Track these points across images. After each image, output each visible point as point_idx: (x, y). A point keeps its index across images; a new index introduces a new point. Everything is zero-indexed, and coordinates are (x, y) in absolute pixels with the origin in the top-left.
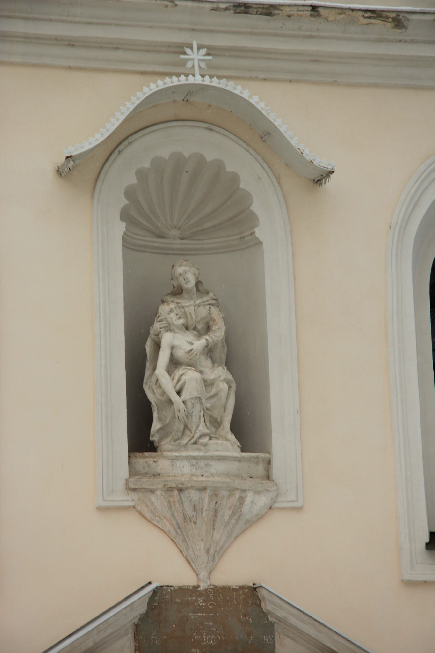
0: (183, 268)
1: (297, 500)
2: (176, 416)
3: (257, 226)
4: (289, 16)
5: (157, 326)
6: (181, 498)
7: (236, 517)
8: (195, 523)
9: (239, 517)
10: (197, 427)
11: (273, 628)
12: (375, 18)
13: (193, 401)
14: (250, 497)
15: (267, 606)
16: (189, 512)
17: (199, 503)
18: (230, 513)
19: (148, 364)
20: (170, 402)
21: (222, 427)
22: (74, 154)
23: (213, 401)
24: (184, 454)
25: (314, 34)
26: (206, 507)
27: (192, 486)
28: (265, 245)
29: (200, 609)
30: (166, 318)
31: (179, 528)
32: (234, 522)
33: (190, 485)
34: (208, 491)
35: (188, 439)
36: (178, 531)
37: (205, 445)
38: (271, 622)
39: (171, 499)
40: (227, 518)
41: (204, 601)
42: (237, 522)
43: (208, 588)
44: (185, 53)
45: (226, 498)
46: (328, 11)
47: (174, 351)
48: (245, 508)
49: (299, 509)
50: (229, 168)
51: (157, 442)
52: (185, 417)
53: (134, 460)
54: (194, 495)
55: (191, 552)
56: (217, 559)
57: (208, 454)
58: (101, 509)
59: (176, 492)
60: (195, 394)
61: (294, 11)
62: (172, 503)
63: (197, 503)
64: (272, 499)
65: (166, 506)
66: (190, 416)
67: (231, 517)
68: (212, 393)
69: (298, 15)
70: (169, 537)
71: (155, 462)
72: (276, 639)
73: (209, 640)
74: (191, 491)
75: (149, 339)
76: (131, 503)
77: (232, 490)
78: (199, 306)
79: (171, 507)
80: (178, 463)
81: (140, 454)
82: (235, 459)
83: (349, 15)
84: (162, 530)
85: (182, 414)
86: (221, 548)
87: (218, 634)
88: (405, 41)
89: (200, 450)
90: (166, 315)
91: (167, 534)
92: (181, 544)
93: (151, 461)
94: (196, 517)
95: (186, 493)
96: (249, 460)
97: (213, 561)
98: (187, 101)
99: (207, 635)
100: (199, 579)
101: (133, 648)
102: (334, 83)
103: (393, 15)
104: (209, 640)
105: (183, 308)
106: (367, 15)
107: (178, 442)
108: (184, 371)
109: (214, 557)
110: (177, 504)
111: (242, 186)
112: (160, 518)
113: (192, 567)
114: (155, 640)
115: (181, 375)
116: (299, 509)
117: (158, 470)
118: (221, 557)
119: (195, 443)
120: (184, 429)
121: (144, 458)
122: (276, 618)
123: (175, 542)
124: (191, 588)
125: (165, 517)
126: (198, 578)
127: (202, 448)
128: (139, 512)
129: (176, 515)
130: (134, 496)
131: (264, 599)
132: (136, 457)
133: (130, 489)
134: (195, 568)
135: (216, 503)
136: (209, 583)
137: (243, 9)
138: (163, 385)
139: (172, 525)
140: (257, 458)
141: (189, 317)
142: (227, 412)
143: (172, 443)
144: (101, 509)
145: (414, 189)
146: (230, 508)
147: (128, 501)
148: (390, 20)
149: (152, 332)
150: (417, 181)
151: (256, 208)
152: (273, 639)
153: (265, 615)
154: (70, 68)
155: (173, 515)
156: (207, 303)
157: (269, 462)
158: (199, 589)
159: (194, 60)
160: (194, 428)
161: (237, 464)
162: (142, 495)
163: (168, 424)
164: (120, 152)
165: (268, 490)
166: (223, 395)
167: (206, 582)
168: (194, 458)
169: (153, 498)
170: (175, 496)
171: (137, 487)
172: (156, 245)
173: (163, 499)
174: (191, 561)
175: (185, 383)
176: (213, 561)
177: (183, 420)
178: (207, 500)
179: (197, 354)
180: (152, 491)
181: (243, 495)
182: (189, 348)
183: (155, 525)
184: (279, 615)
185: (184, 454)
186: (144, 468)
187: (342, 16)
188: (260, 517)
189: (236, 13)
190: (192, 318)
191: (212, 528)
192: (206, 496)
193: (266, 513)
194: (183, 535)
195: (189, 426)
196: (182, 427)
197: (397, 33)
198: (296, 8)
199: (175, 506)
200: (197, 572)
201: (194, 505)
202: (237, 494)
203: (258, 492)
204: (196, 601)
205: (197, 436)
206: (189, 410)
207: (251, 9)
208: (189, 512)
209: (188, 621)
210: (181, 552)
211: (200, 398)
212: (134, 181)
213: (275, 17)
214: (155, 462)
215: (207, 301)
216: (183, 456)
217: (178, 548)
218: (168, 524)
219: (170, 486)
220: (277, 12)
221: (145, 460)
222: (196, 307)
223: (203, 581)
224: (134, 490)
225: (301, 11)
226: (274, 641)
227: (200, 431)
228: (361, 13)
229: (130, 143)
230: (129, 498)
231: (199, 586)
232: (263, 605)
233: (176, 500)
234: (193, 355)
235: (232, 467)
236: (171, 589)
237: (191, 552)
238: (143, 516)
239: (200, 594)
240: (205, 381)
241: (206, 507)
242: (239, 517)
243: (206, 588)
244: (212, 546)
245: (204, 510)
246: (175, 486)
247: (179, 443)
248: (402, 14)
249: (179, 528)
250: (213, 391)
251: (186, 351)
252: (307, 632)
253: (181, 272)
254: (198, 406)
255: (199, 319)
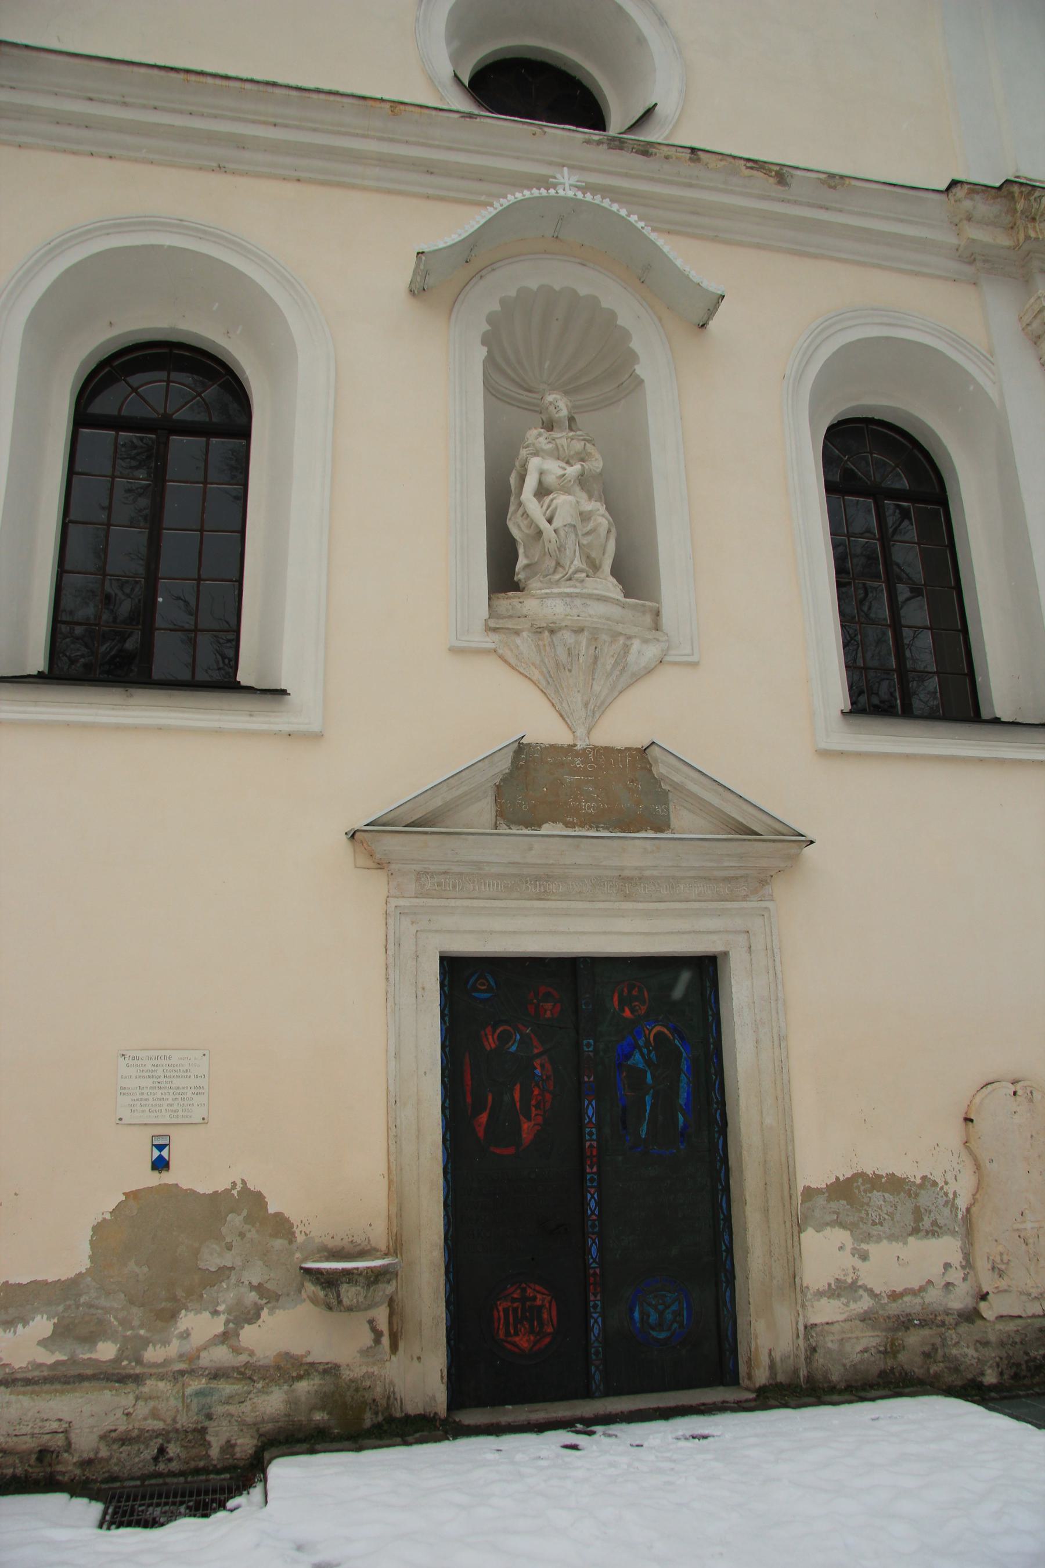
0: (554, 396)
1: (693, 655)
2: (546, 550)
3: (638, 363)
4: (667, 158)
5: (523, 452)
6: (552, 641)
7: (620, 668)
8: (570, 671)
9: (624, 668)
10: (572, 563)
11: (668, 798)
12: (757, 169)
13: (566, 529)
14: (636, 645)
15: (660, 770)
16: (563, 657)
17: (575, 648)
18: (613, 662)
19: (512, 499)
20: (540, 533)
21: (601, 570)
22: (426, 250)
23: (590, 538)
24: (556, 590)
25: (694, 182)
26: (583, 652)
27: (566, 626)
28: (647, 384)
29: (577, 772)
30: (534, 444)
31: (551, 677)
32: (618, 673)
33: (564, 624)
34: (586, 633)
35: (561, 575)
36: (549, 680)
37: (582, 581)
38: (665, 790)
39: (540, 643)
40: (609, 667)
41: (582, 762)
42: (621, 674)
43: (587, 748)
44: (555, 178)
45: (607, 644)
46: (708, 155)
47: (543, 478)
48: (631, 658)
49: (695, 665)
50: (604, 305)
51: (523, 581)
52: (556, 549)
53: (495, 602)
54: (568, 637)
55: (565, 705)
56: (597, 716)
57: (585, 591)
58: (454, 650)
59: (547, 633)
60: (569, 520)
61: (671, 152)
62: (542, 647)
63: (573, 646)
64: (663, 650)
65: (534, 650)
66: (563, 549)
67: (614, 667)
68: (588, 528)
69: (677, 158)
70: (538, 687)
71: (520, 602)
72: (671, 810)
73: (589, 808)
74: (565, 632)
75: (514, 471)
76: (493, 646)
77: (615, 635)
78: (572, 439)
79: (540, 651)
80: (549, 602)
81: (503, 594)
82: (617, 602)
83: (731, 163)
84: (529, 678)
85: (552, 547)
86: (602, 703)
87: (600, 801)
88: (789, 201)
89: (576, 587)
90: (534, 441)
91: (535, 684)
92: (553, 695)
93: (515, 602)
94: (572, 664)
95: (559, 635)
96: (634, 607)
97: (593, 718)
98: (557, 237)
99: (586, 802)
100: (575, 737)
101: (494, 814)
102: (715, 239)
103: (777, 168)
104: (589, 808)
105: (554, 440)
106: (749, 164)
107: (548, 577)
108: (555, 495)
109: (594, 712)
110: (548, 648)
111: (619, 322)
112: (527, 664)
113: (567, 723)
114: (521, 805)
115: (552, 500)
116: (695, 665)
117: (525, 612)
118: (603, 713)
119: (570, 579)
120: (556, 568)
121: (507, 599)
122: (671, 785)
123: (545, 694)
124: (565, 746)
125: (533, 664)
126: (574, 736)
127: (578, 584)
128: (501, 657)
129: (546, 661)
130: (495, 637)
131: (656, 761)
132: (498, 598)
133: (489, 629)
134: (570, 724)
135: (596, 648)
136: (587, 742)
137: (617, 143)
138: (530, 512)
139: (542, 673)
140: (643, 605)
141: (561, 449)
142: (606, 555)
143: (541, 579)
144: (454, 650)
145: (805, 345)
146: (613, 656)
147: (487, 642)
148: (774, 173)
149: (517, 464)
150: (809, 337)
151: (635, 344)
152: (668, 810)
153: (656, 782)
154: (428, 197)
155: (542, 661)
156: (582, 438)
157: (658, 614)
158: (576, 748)
159: (564, 184)
160: (568, 564)
161: (620, 609)
162: (504, 636)
163: (536, 563)
164: (481, 277)
165: (658, 640)
166: (603, 531)
167: (584, 741)
168: (569, 595)
169: (518, 641)
170: (546, 638)
171: (498, 626)
172: (521, 397)
173: (531, 642)
174: (565, 716)
175: (556, 508)
176: (593, 718)
177: (554, 553)
178: (584, 643)
179: (570, 481)
180: (517, 633)
181: (629, 643)
182: (560, 472)
183: (521, 673)
184: (675, 780)
185: (556, 590)
186: (507, 610)
187: (723, 163)
188: (649, 671)
189: (610, 148)
190: (564, 450)
191: (591, 678)
192: (583, 639)
193: (656, 666)
194: (556, 686)
195: (562, 562)
196: (553, 564)
197: (778, 191)
198: (674, 149)
199: (545, 651)
200: (573, 728)
201: (569, 649)
202: (621, 640)
203: (645, 641)
204: (573, 762)
205: (571, 571)
206: (562, 541)
207: (626, 145)
208: (563, 657)
209: (563, 784)
210: (553, 705)
211: (574, 526)
212: (497, 308)
213: (651, 158)
214: (520, 602)
215: (582, 436)
216: (555, 594)
217: (550, 700)
218: (536, 672)
219: (539, 626)
220: (654, 150)
221: (509, 601)
222: (569, 440)
223: (581, 740)
224: (495, 630)
225: (679, 152)
226: (669, 812)
227: (575, 565)
228: (743, 162)
229: (493, 270)
230: (488, 639)
231: (575, 745)
232: (654, 769)
233: (546, 642)
234: (566, 481)
235: (615, 611)
236: (540, 747)
237: (565, 705)
238: (506, 662)
239: (577, 754)
240: (581, 514)
241: (583, 652)
242: (624, 668)
243: (585, 747)
244: (592, 699)
245: (581, 655)
246: (545, 625)
247: (550, 579)
248: (785, 169)
249: (551, 677)
250: (591, 525)
251: (558, 475)
252: (708, 800)
253: (551, 400)
254: (573, 536)
255: (572, 453)
